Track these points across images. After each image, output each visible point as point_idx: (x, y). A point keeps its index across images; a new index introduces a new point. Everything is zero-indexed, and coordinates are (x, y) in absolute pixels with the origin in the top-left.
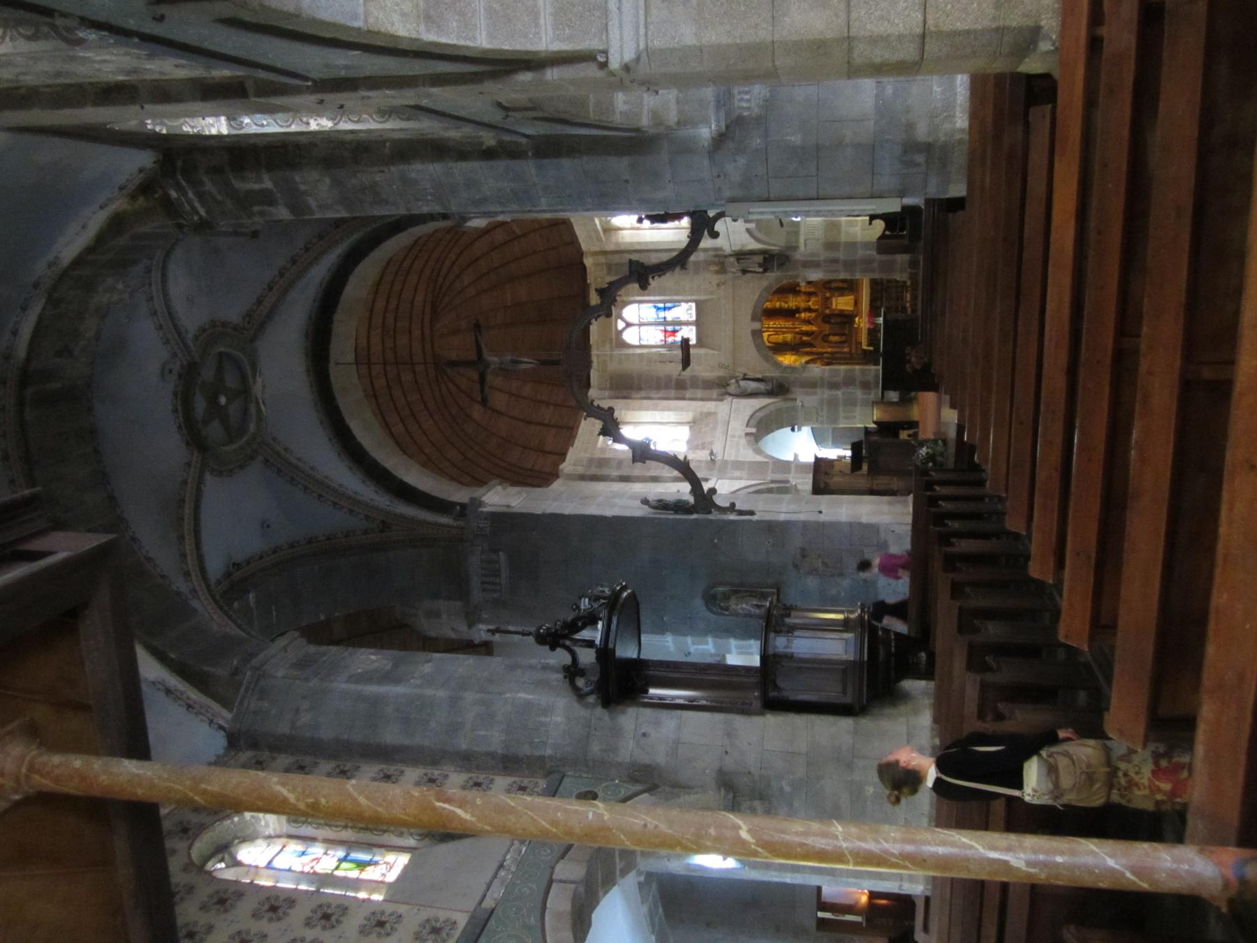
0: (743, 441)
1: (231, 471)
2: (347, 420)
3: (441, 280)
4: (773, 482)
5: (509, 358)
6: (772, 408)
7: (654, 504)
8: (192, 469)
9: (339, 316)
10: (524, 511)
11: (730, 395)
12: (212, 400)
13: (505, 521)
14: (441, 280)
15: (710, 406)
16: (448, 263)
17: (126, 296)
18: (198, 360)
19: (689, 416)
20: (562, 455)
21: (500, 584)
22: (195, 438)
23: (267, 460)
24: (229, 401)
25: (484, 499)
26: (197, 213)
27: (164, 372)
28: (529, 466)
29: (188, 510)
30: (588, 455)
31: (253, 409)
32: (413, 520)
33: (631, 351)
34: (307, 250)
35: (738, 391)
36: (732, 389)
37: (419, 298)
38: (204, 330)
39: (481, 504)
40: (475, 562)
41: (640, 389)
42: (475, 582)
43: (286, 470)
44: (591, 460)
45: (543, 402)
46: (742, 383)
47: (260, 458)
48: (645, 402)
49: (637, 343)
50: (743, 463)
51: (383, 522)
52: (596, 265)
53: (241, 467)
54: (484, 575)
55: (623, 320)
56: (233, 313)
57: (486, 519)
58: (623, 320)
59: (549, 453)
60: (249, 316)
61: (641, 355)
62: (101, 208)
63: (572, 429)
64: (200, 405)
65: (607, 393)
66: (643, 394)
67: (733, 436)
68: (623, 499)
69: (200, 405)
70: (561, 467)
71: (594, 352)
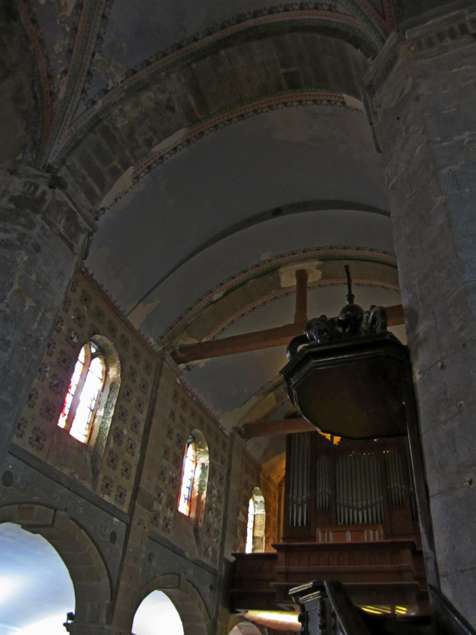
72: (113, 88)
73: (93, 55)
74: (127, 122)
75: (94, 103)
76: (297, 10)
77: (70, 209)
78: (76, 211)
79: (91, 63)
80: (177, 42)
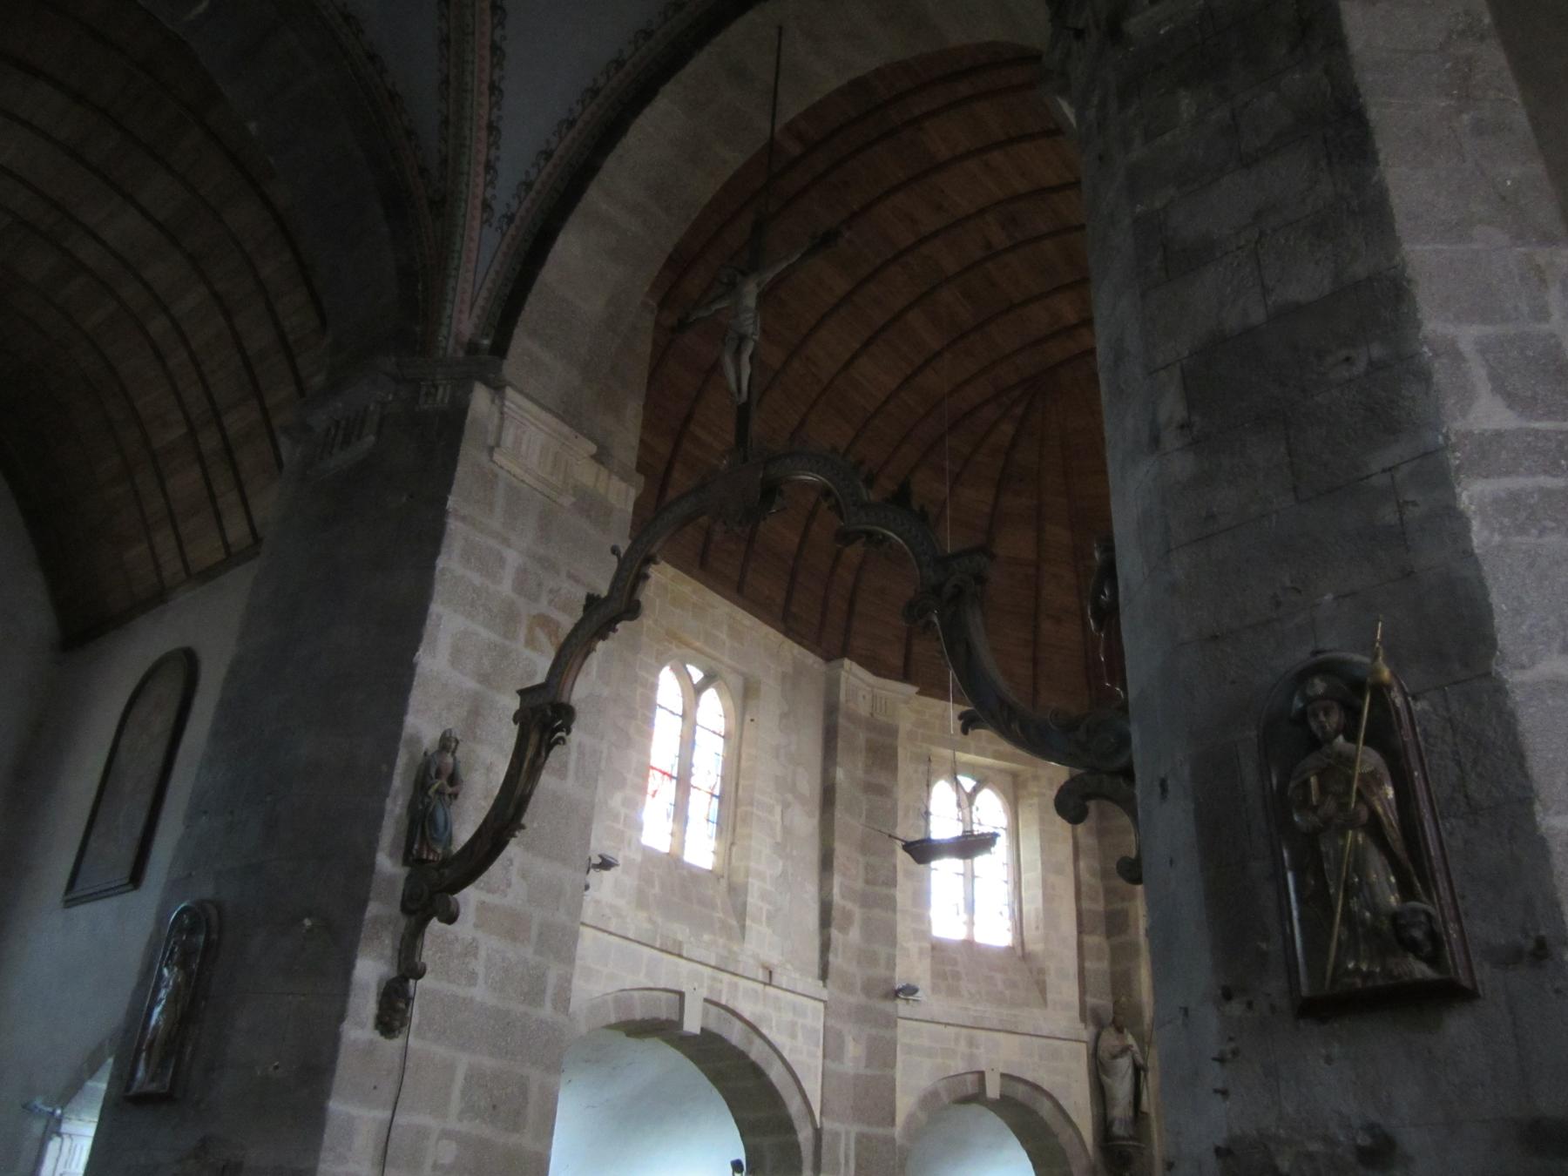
0: (958, 1066)
4: (818, 1133)
6: (1065, 1136)
11: (1098, 1037)
15: (1066, 990)
19: (1035, 946)
35: (1104, 1054)
36: (1110, 1040)
46: (1124, 1064)
50: (890, 1063)
51: (1541, 944)
67: (971, 1043)
68: (460, 678)
70: (847, 662)
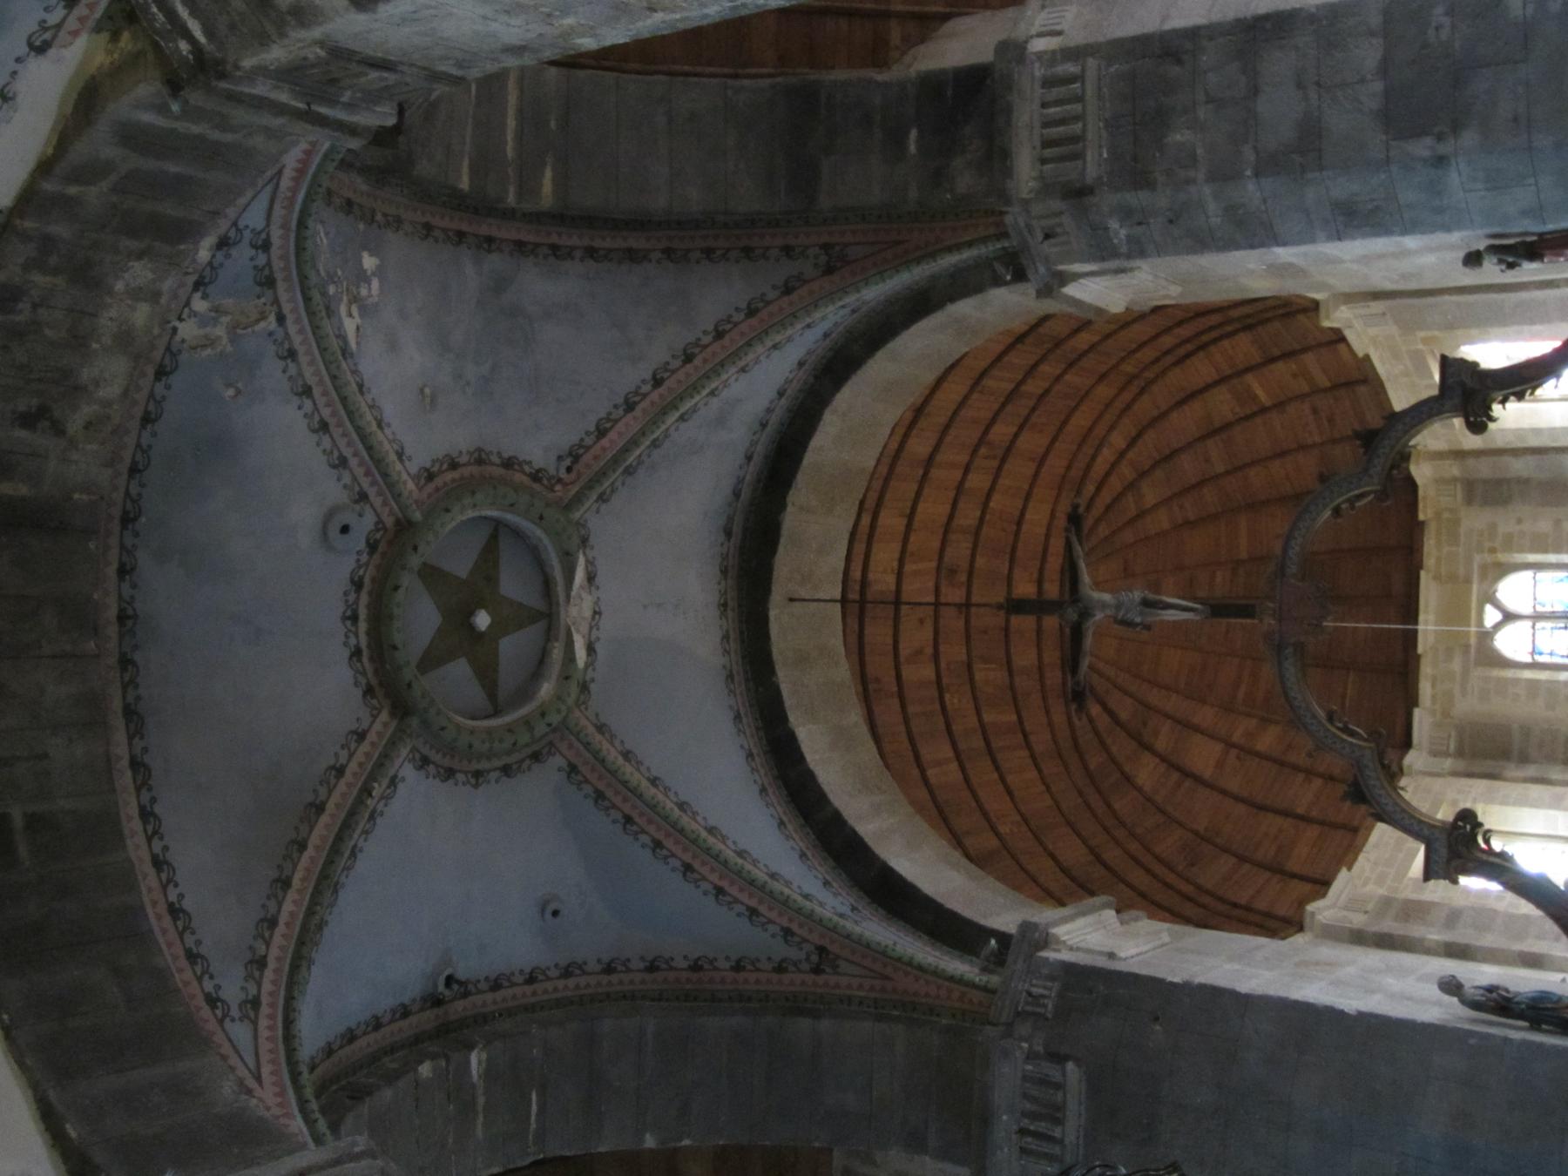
1: (478, 774)
2: (793, 718)
3: (1090, 488)
5: (1137, 595)
7: (1479, 996)
8: (365, 747)
9: (801, 495)
10: (1144, 972)
12: (458, 618)
13: (1093, 985)
14: (1090, 488)
16: (1107, 455)
17: (220, 331)
18: (417, 516)
20: (1322, 885)
21: (1060, 1142)
22: (388, 685)
23: (573, 769)
24: (500, 627)
25: (1061, 931)
26: (188, 35)
27: (333, 528)
28: (1243, 902)
29: (322, 832)
30: (1382, 891)
31: (557, 653)
32: (883, 954)
33: (1510, 673)
34: (719, 335)
37: (1037, 516)
38: (454, 465)
39: (1046, 941)
40: (1007, 1077)
41: (1524, 759)
42: (1005, 1125)
43: (618, 799)
44: (1387, 902)
45: (1296, 768)
47: (558, 761)
48: (1536, 790)
49: (1528, 659)
52: (1440, 481)
53: (506, 770)
54: (1024, 1114)
55: (1498, 605)
56: (539, 445)
57: (1052, 978)
58: (1498, 605)
59: (1294, 876)
60: (574, 455)
61: (1533, 685)
62: (40, 49)
63: (1355, 830)
64: (420, 618)
65: (1448, 763)
66: (1531, 770)
69: (420, 618)
70: (1310, 908)
71: (1426, 669)
72: (187, 304)
73: (281, 319)
74: (119, 286)
75: (223, 243)
76: (166, 895)
77: (332, 102)
78: (315, 108)
79: (276, 301)
80: (143, 519)
